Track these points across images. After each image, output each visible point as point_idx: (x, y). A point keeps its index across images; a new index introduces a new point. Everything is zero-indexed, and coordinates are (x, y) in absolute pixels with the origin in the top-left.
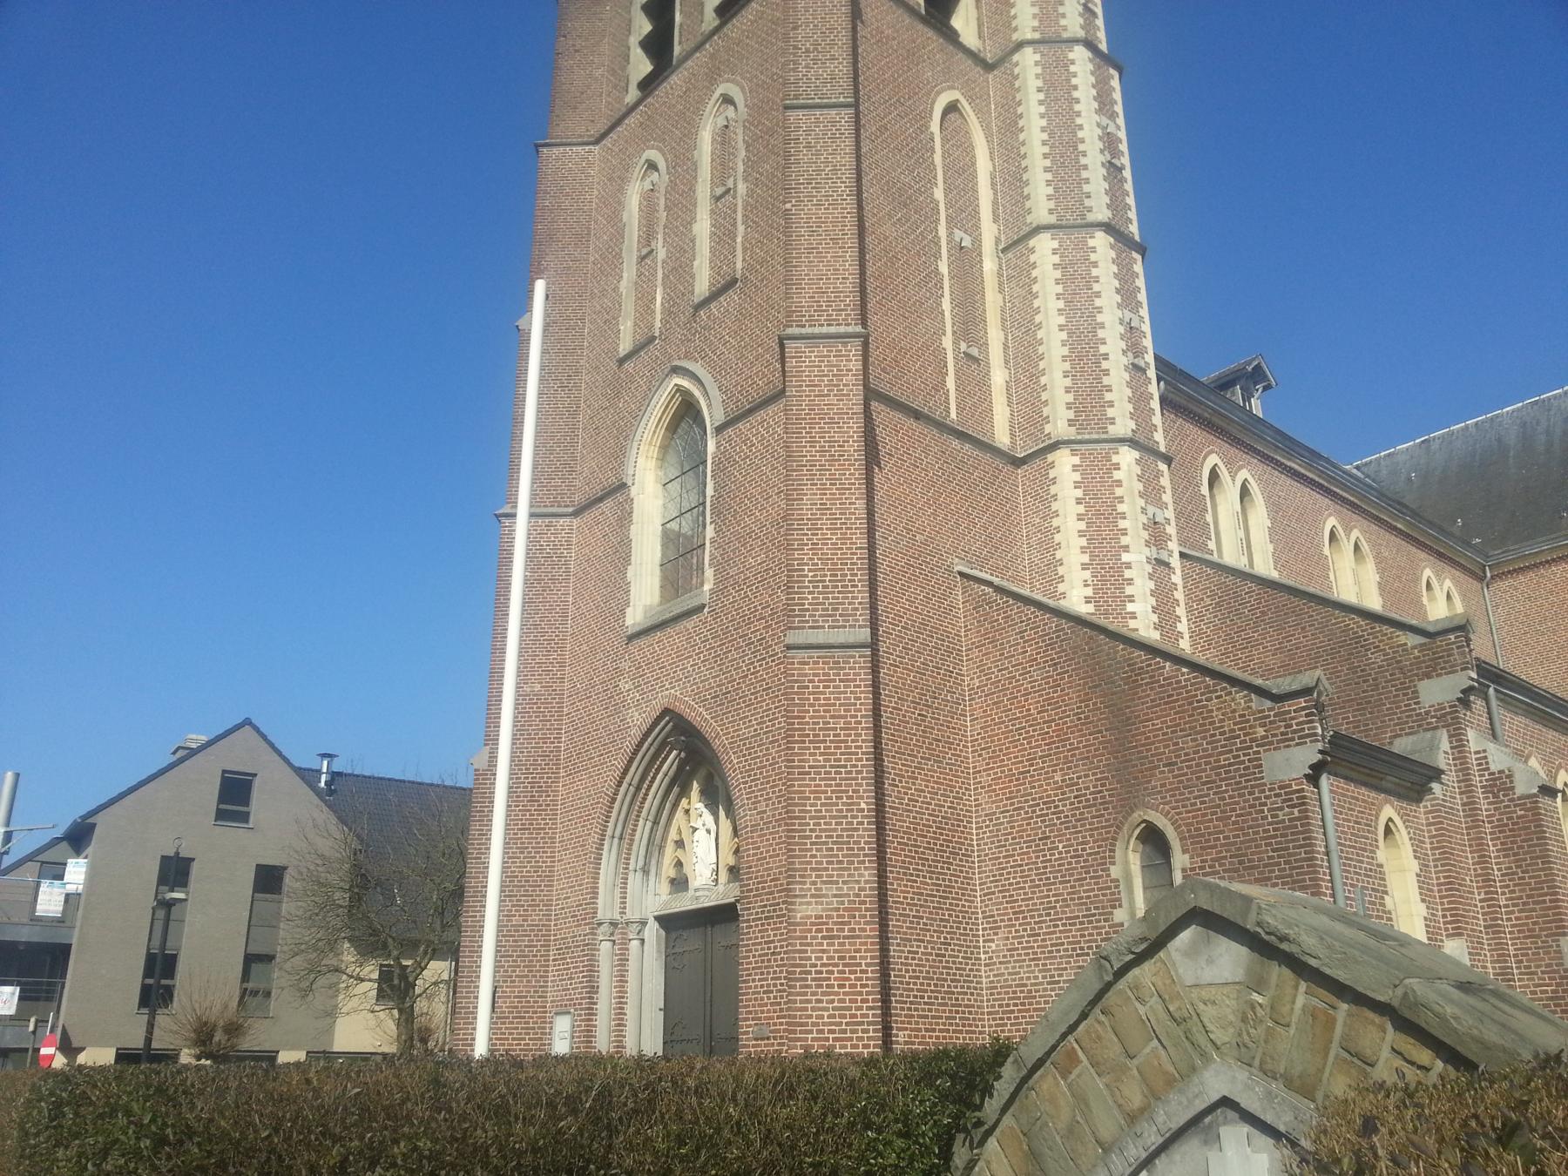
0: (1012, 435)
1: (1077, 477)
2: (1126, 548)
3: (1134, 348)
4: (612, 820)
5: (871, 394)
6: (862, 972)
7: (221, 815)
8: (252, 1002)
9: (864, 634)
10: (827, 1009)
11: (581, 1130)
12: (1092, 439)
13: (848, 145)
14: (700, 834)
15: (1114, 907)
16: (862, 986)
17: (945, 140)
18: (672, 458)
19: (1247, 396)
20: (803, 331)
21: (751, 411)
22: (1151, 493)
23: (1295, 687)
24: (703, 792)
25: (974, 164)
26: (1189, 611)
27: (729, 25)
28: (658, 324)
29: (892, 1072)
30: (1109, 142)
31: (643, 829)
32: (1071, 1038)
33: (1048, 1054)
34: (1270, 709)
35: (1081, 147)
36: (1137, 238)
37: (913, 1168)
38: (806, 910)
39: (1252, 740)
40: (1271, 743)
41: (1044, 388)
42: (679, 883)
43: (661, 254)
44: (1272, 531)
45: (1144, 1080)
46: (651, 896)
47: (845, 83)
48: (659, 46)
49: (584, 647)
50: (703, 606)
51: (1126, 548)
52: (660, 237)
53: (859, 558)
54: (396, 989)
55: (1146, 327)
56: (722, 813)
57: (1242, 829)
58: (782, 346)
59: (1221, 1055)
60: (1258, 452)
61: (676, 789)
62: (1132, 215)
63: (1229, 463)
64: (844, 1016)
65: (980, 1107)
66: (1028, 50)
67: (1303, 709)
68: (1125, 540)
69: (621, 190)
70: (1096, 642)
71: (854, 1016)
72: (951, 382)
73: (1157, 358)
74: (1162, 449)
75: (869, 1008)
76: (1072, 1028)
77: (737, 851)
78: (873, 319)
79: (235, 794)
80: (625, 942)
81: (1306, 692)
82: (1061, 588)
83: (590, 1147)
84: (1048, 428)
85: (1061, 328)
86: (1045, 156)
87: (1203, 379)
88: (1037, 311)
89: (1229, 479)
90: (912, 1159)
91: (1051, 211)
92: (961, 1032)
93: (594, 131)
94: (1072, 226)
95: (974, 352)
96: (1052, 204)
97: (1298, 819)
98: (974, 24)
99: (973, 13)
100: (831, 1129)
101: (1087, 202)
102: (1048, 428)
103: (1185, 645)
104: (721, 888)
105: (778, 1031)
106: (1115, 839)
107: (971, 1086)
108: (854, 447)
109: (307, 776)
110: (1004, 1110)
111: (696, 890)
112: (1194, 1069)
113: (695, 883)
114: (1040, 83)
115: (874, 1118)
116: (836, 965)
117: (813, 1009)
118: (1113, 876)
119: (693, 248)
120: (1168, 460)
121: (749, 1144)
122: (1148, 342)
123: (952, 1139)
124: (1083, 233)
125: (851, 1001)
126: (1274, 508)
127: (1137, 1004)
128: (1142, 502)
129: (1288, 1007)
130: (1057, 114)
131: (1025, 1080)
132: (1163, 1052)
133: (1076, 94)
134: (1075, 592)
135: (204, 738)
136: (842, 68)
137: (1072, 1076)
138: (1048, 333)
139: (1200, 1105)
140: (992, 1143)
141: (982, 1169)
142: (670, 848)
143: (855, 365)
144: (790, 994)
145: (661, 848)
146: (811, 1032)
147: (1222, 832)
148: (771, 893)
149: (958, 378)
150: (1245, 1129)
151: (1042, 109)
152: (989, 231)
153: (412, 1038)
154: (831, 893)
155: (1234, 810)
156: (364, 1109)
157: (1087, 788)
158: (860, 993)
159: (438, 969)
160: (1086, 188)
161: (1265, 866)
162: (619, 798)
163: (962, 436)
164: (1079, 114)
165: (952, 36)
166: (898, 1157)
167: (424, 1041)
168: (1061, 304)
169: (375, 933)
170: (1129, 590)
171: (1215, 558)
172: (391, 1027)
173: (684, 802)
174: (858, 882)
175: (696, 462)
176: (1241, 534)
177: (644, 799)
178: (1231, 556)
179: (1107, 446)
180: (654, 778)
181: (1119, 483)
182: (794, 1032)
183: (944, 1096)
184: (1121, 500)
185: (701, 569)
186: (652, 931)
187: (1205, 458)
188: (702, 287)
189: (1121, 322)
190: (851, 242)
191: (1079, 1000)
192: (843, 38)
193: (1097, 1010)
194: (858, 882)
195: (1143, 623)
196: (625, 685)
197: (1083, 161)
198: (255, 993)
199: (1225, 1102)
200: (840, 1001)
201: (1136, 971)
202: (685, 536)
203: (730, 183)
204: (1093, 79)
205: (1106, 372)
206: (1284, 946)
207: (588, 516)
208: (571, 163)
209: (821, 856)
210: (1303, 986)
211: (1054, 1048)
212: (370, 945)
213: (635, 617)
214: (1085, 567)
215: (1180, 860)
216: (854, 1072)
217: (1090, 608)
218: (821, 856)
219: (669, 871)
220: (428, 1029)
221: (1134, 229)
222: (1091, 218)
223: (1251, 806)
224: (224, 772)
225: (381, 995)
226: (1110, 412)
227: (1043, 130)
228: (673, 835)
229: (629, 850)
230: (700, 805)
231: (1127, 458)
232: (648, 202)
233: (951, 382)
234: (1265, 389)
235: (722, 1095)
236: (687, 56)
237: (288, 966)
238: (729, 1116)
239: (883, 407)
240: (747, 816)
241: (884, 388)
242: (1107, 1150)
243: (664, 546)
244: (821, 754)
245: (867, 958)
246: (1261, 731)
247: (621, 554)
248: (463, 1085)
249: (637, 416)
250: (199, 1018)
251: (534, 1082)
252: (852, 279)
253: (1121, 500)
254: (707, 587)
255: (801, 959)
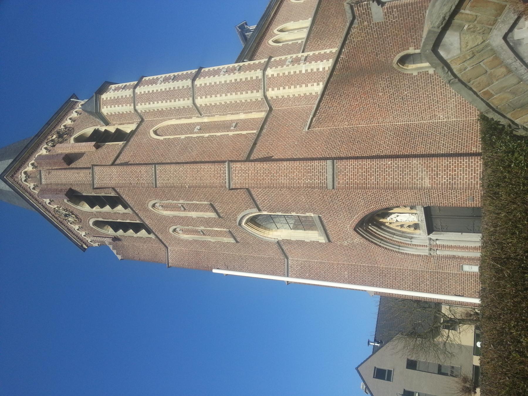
0: (262, 111)
1: (276, 89)
2: (300, 71)
3: (233, 70)
4: (393, 249)
5: (248, 160)
6: (450, 163)
7: (389, 379)
8: (455, 373)
9: (329, 162)
10: (463, 176)
11: (508, 268)
12: (263, 84)
13: (167, 167)
14: (399, 219)
15: (428, 74)
16: (455, 163)
17: (166, 135)
18: (269, 226)
19: (249, 31)
20: (227, 182)
21: (254, 200)
22: (282, 63)
23: (350, 11)
24: (384, 218)
25: (173, 125)
26: (322, 49)
27: (130, 205)
28: (225, 230)
29: (489, 157)
30: (166, 80)
31: (396, 238)
32: (479, 93)
33: (484, 101)
34: (358, 20)
35: (168, 89)
36: (197, 70)
37: (526, 150)
38: (427, 183)
39: (369, 26)
40: (370, 19)
41: (246, 101)
42: (416, 226)
43: (202, 228)
44: (295, 21)
45: (495, 67)
46: (420, 236)
47: (148, 167)
48: (137, 227)
49: (332, 257)
50: (319, 216)
51: (300, 71)
52: (197, 228)
53: (303, 164)
54: (452, 324)
55: (226, 66)
56: (391, 211)
57: (400, 29)
58: (232, 189)
59: (487, 40)
60: (268, 27)
61: (382, 227)
62: (189, 72)
63: (272, 36)
64: (466, 170)
65: (504, 126)
66: (137, 107)
67: (358, 8)
68: (298, 72)
69: (182, 240)
70: (334, 81)
71: (466, 166)
72: (244, 132)
73: (236, 63)
74: (267, 60)
75: (463, 161)
76: (475, 93)
77: (405, 206)
78: (223, 159)
79: (381, 374)
80: (437, 245)
81: (352, 8)
82: (314, 94)
83: (515, 265)
84: (260, 99)
85: (226, 95)
86: (171, 101)
87: (243, 46)
88: (221, 103)
89: (277, 36)
90: (522, 150)
91: (188, 99)
92: (473, 128)
93: (164, 249)
94: (193, 93)
95: (234, 124)
96: (186, 99)
97: (397, 9)
98: (129, 125)
99: (125, 126)
100: (511, 180)
101: (185, 87)
102: (260, 99)
103: (335, 50)
104: (418, 212)
105: (471, 193)
106: (403, 74)
107: (495, 129)
108: (266, 165)
109: (375, 350)
110: (504, 117)
111: (419, 221)
112: (492, 49)
113: (416, 221)
114: (147, 103)
115: (507, 164)
116: (447, 172)
117: (463, 181)
118: (417, 74)
119: (201, 217)
120: (270, 58)
121: (515, 209)
122: (231, 66)
123: (515, 135)
124: (195, 89)
125: (461, 167)
126: (287, 20)
127: (467, 70)
128: (285, 66)
129: (469, 16)
130: (157, 98)
131: (494, 109)
132: (485, 61)
133: (151, 92)
134: (315, 89)
135: (362, 383)
136: (143, 168)
137: (493, 93)
138: (228, 100)
139: (506, 47)
140: (517, 121)
141: (526, 125)
142: (403, 229)
143: (238, 165)
144: (458, 189)
145: (403, 232)
146: (472, 182)
147: (401, 36)
148: (420, 195)
149: (242, 130)
150: (516, 30)
151: (156, 102)
152: (195, 120)
153: (470, 320)
154: (422, 175)
155: (394, 32)
156: (499, 344)
157: (385, 84)
158: (458, 164)
159: (445, 310)
160: (181, 88)
161: (414, 20)
162: (385, 246)
163: (262, 128)
164: (157, 90)
165: (133, 132)
166: (521, 155)
167: (471, 315)
168: (218, 95)
169: (432, 330)
170: (315, 70)
171: (304, 40)
172: (465, 326)
173: (387, 224)
174: (417, 165)
175: (270, 218)
176: (296, 31)
177: (386, 238)
178: (304, 35)
179: (266, 79)
180: (378, 234)
181: (278, 74)
182: (471, 188)
183: (499, 138)
184: (284, 74)
185: (306, 217)
186: (433, 236)
187: (270, 45)
188: (213, 215)
189: (224, 75)
190: (198, 166)
191: (465, 90)
192: (134, 168)
193: (469, 84)
194: (417, 165)
195: (327, 65)
196: (346, 243)
197: (172, 89)
198: (452, 372)
199: (505, 38)
200: (461, 171)
201: (455, 71)
202: (295, 222)
203: (180, 205)
204: (146, 86)
205: (241, 80)
206: (447, 18)
207: (288, 254)
208: (174, 256)
209: (407, 178)
210: (462, 11)
211: (482, 99)
212: (435, 332)
213: (322, 239)
214: (307, 86)
215: (411, 50)
216: (489, 171)
217: (321, 84)
218: (407, 178)
219: (412, 230)
220: (467, 314)
221: (194, 71)
222: (190, 86)
223: (392, 26)
224: (374, 377)
225: (454, 329)
226: (254, 78)
227: (162, 102)
228: (399, 228)
229: (404, 243)
230: (388, 219)
231: (270, 72)
232: (183, 230)
233: (244, 132)
234: (247, 25)
235: (496, 218)
236: (140, 218)
237: (443, 361)
238: (505, 216)
239: (252, 156)
240: (392, 203)
241: (246, 155)
242: (521, 80)
243: (298, 229)
244: (371, 177)
245: (445, 161)
246: (366, 23)
247: (301, 243)
248: (490, 309)
249: (255, 237)
250: (461, 391)
251: (490, 284)
252: (211, 166)
253: (284, 74)
254: (312, 215)
255: (445, 185)
